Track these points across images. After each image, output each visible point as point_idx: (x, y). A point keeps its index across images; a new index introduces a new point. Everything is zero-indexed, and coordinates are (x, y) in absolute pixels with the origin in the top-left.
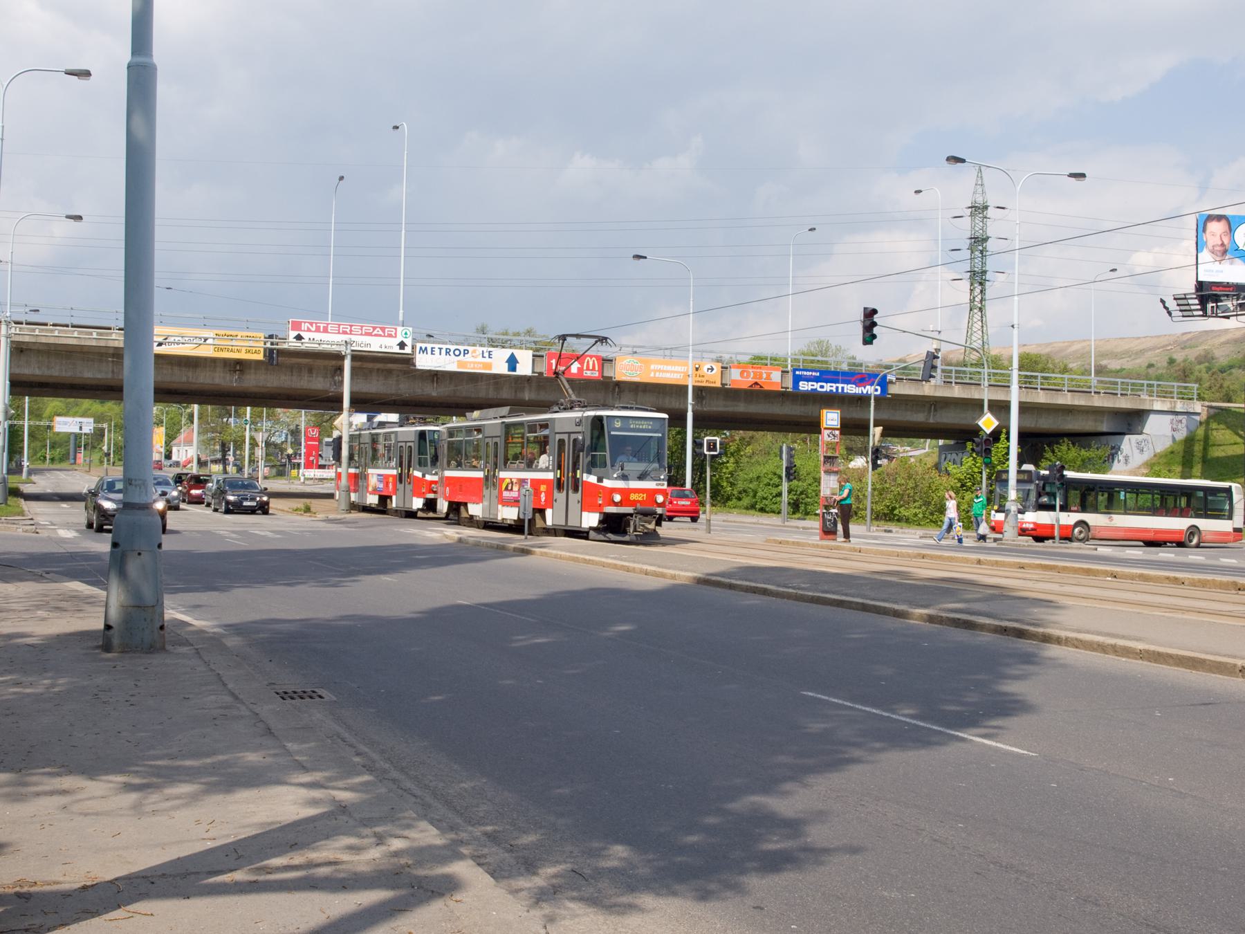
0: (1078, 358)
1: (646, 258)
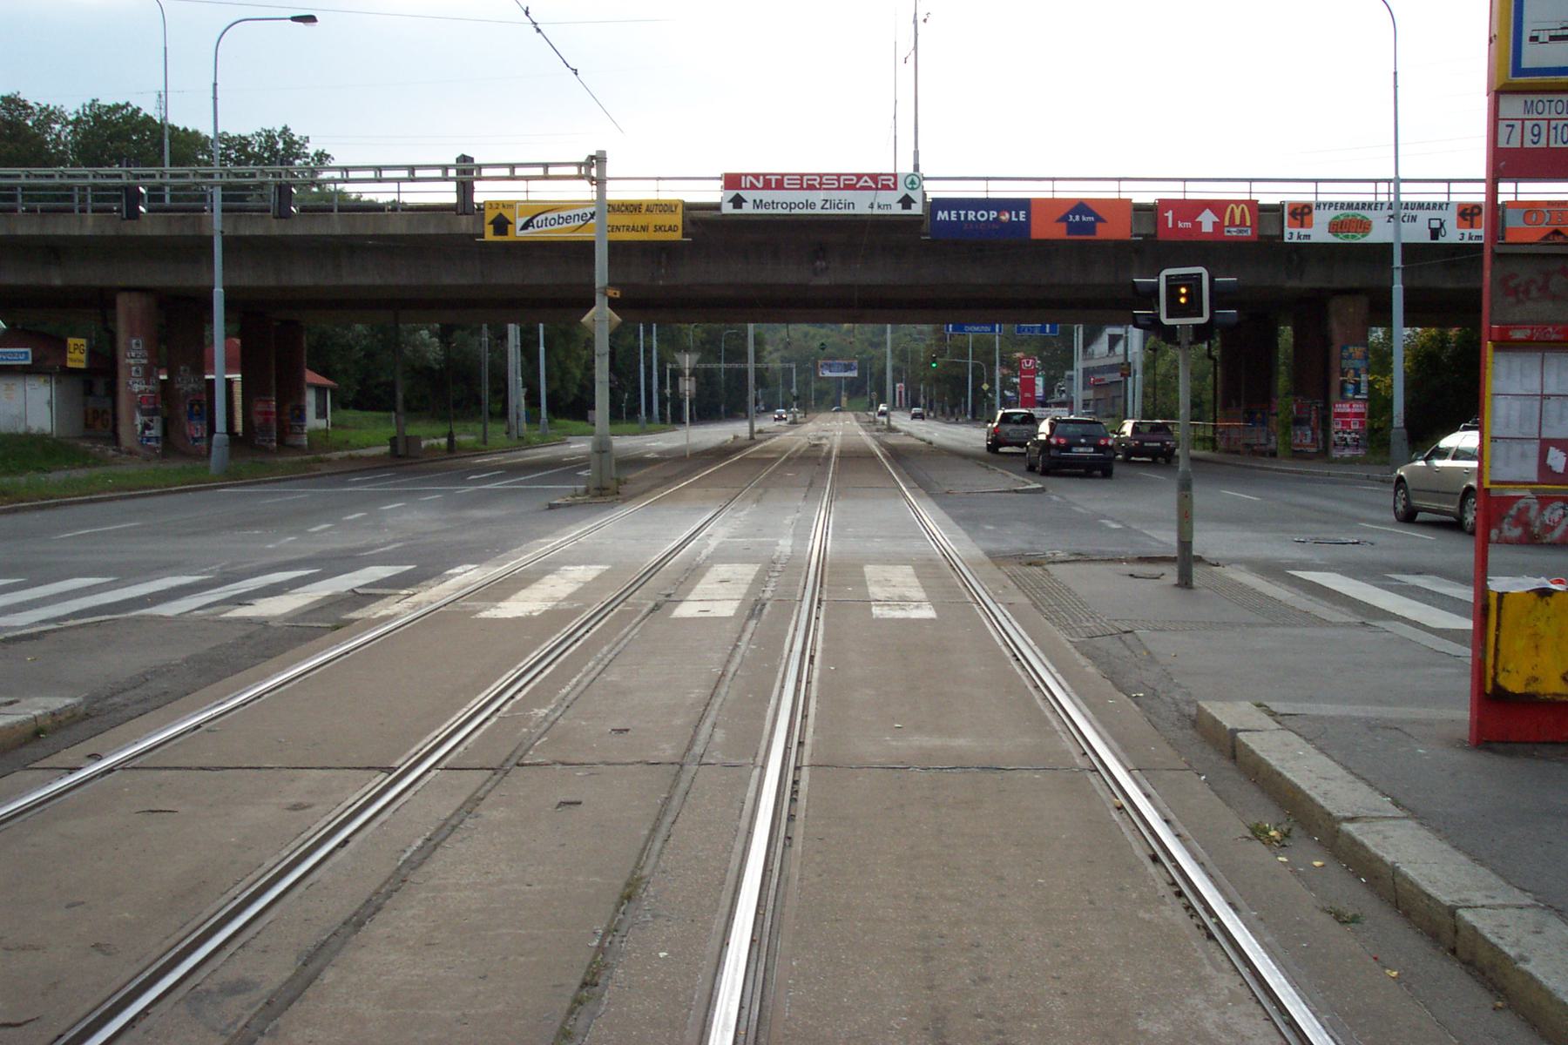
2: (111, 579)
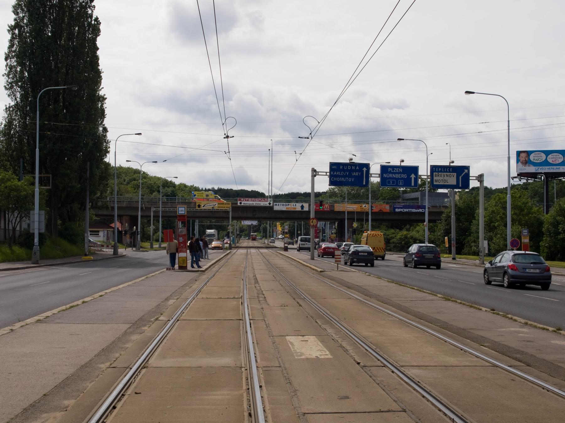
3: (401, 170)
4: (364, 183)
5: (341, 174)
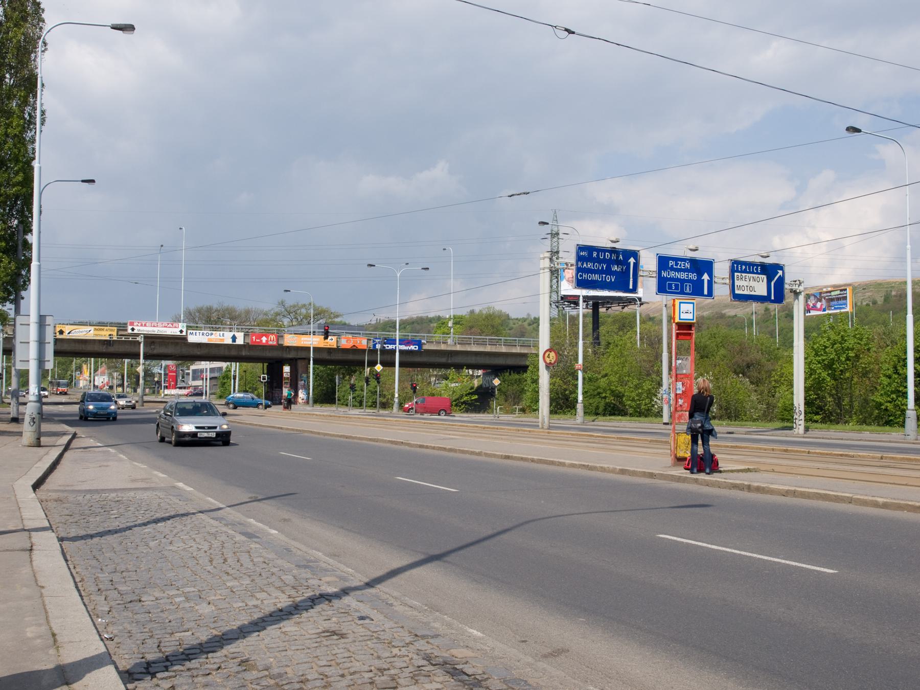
0: (710, 308)
1: (374, 266)
2: (661, 536)
3: (688, 266)
4: (631, 287)
5: (593, 267)
